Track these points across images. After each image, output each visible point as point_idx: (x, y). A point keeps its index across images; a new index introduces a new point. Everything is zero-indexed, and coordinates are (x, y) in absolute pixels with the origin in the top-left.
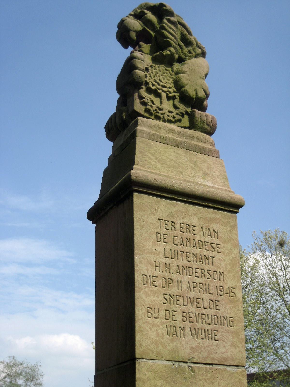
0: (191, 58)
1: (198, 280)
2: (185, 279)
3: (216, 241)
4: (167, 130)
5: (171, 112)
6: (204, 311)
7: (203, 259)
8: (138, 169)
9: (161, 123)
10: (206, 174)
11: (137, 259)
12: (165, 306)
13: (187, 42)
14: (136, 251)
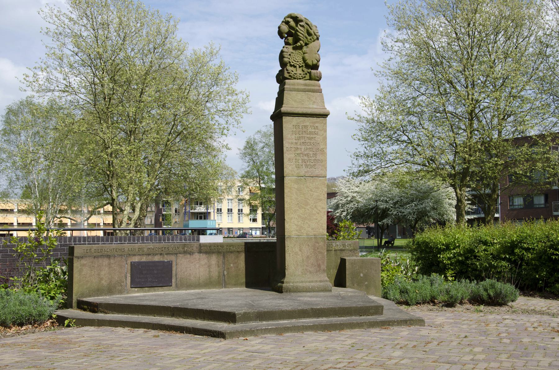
0: (311, 42)
1: (308, 147)
2: (303, 147)
3: (317, 131)
4: (298, 84)
5: (300, 74)
6: (310, 158)
7: (310, 139)
8: (285, 107)
9: (296, 81)
10: (314, 102)
11: (284, 142)
12: (295, 158)
13: (309, 34)
14: (284, 139)
